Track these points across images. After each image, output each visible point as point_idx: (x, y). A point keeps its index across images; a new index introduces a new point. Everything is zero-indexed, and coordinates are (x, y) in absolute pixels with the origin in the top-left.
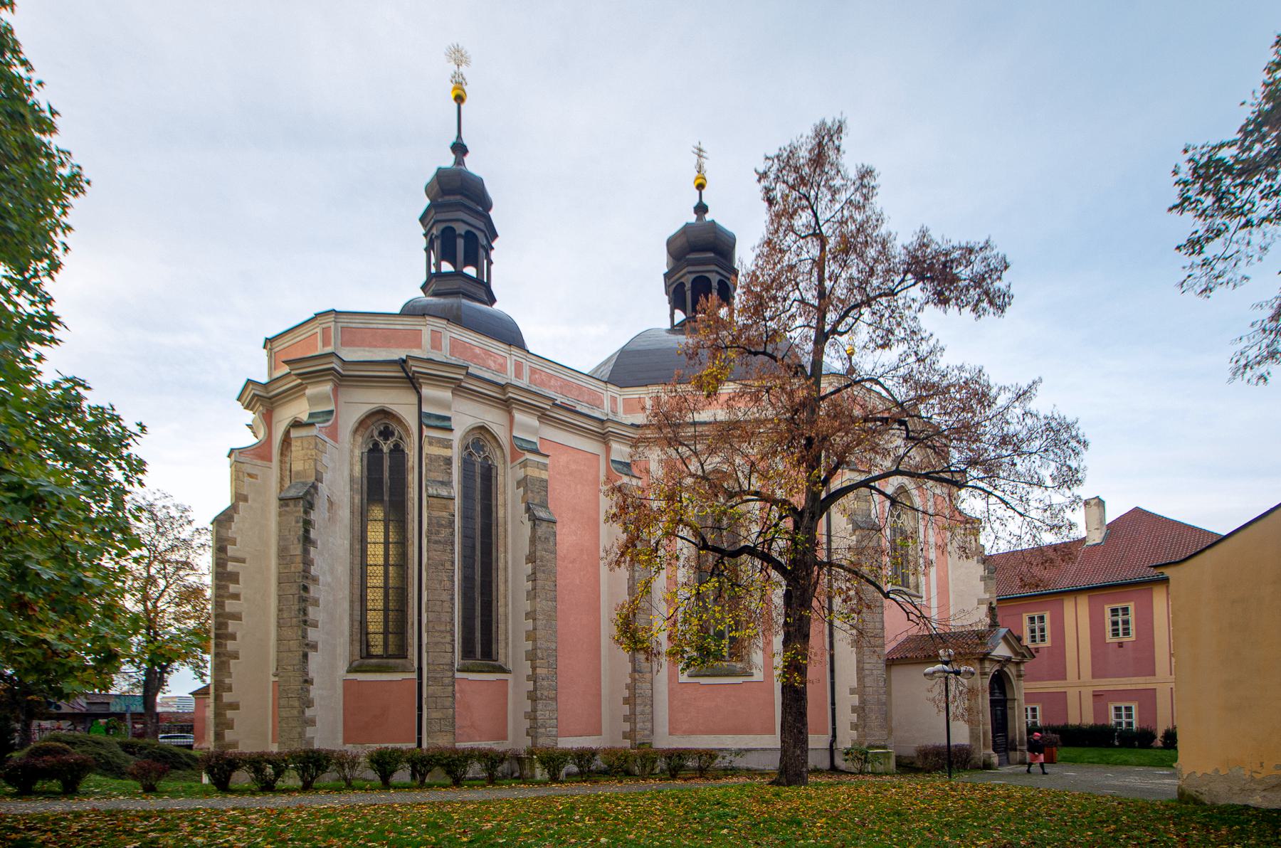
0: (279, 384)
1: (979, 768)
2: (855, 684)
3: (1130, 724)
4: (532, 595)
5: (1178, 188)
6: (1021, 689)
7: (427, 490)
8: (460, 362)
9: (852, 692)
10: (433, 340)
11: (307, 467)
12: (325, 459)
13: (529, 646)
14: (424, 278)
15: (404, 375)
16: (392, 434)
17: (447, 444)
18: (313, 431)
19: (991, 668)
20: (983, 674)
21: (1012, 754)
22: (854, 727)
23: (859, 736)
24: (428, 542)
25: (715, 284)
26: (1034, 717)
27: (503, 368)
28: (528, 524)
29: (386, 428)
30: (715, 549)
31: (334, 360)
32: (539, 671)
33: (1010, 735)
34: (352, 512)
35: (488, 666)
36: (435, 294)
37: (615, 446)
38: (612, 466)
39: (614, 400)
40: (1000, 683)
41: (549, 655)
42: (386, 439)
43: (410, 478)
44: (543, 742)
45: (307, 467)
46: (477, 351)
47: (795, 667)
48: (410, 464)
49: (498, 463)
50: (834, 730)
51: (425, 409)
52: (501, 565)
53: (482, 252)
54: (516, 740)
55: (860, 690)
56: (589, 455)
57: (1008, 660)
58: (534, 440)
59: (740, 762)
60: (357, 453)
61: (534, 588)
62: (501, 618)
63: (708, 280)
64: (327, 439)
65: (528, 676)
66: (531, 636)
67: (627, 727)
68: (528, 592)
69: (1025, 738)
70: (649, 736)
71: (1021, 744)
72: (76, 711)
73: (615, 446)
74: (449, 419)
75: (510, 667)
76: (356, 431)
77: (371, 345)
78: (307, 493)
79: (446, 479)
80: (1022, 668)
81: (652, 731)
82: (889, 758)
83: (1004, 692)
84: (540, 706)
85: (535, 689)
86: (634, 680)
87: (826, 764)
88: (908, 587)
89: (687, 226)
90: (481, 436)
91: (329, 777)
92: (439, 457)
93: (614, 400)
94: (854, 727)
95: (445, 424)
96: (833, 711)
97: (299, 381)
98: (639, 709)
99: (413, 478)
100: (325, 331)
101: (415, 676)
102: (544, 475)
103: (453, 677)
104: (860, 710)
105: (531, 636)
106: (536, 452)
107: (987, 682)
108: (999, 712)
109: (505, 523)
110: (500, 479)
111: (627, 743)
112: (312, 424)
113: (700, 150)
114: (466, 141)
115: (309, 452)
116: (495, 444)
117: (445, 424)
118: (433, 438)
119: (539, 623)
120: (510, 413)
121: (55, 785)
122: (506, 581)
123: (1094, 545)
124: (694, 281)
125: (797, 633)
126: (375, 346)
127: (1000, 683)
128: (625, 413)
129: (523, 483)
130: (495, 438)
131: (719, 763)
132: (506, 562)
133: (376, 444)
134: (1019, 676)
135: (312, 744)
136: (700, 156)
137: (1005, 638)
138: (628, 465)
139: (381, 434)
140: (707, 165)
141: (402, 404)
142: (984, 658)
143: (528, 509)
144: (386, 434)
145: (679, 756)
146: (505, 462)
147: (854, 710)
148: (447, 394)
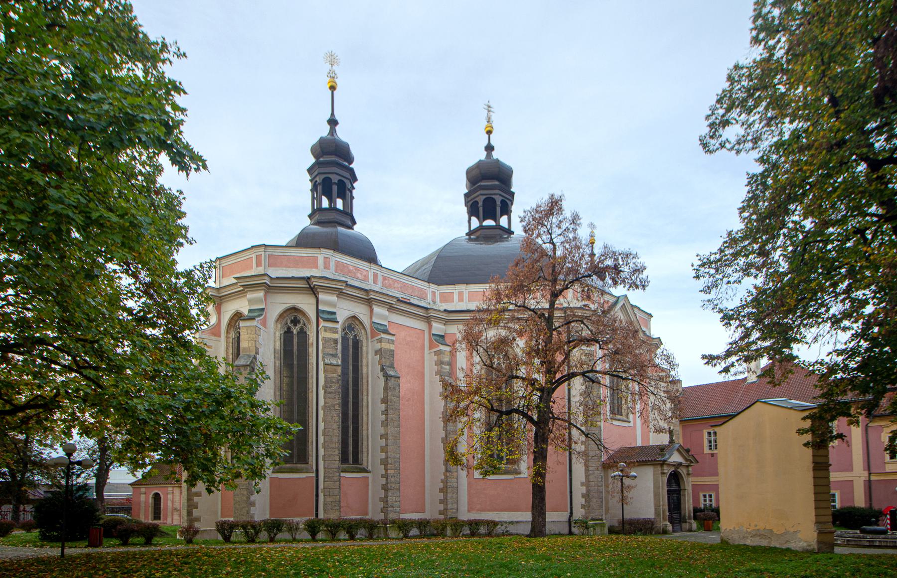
0: (224, 290)
1: (659, 533)
2: (584, 480)
3: (711, 505)
4: (385, 424)
5: (695, 272)
6: (689, 483)
7: (323, 360)
8: (344, 279)
9: (582, 484)
10: (325, 263)
11: (250, 345)
12: (260, 340)
13: (383, 455)
14: (310, 212)
15: (308, 286)
16: (299, 322)
17: (335, 331)
18: (254, 323)
19: (668, 470)
20: (663, 473)
21: (684, 525)
22: (583, 507)
23: (586, 513)
24: (325, 392)
25: (498, 203)
26: (711, 501)
27: (366, 279)
28: (383, 379)
29: (295, 318)
30: (497, 411)
31: (266, 278)
32: (389, 472)
33: (683, 513)
34: (275, 372)
35: (357, 468)
36: (318, 223)
37: (435, 325)
38: (433, 338)
39: (434, 293)
40: (675, 479)
41: (395, 462)
42: (295, 325)
43: (310, 350)
44: (391, 516)
45: (250, 345)
46: (351, 268)
47: (539, 475)
48: (311, 341)
49: (363, 338)
50: (571, 509)
51: (320, 308)
52: (364, 404)
53: (348, 192)
54: (374, 514)
55: (587, 484)
56: (418, 331)
57: (680, 464)
58: (385, 323)
59: (512, 529)
60: (278, 334)
61: (386, 420)
62: (365, 438)
63: (494, 201)
64: (261, 327)
65: (382, 475)
66: (384, 449)
67: (442, 507)
68: (382, 422)
69: (692, 515)
70: (455, 513)
71: (690, 518)
72: (37, 498)
73: (435, 325)
74: (334, 313)
75: (370, 468)
76: (277, 321)
77: (286, 266)
78: (252, 362)
79: (334, 352)
80: (690, 469)
81: (457, 510)
82: (604, 527)
83: (678, 484)
84: (390, 494)
85: (387, 483)
86: (446, 477)
87: (566, 531)
88: (622, 415)
89: (480, 162)
90: (353, 322)
91: (283, 535)
92: (330, 339)
93: (434, 293)
94: (583, 507)
95: (333, 316)
96: (571, 496)
97: (241, 288)
98: (449, 495)
99: (312, 350)
100: (258, 257)
101: (314, 475)
102: (392, 347)
103: (339, 476)
104: (586, 496)
105: (384, 449)
106: (386, 332)
107: (665, 479)
108: (675, 498)
109: (367, 377)
110: (364, 348)
111: (442, 517)
112: (253, 319)
113: (489, 107)
114: (337, 117)
115: (252, 336)
116: (361, 327)
117: (333, 316)
118: (327, 327)
119: (389, 441)
120: (371, 307)
121: (141, 540)
122: (368, 414)
123: (752, 383)
124: (485, 201)
125: (540, 456)
126: (289, 267)
127: (675, 479)
128: (441, 302)
129: (379, 352)
130: (361, 323)
131: (499, 529)
132: (368, 402)
133: (289, 328)
134: (688, 474)
135: (253, 518)
136: (489, 111)
137: (678, 450)
138: (442, 337)
139: (292, 322)
140: (494, 117)
141: (306, 304)
142: (663, 463)
143: (383, 369)
144: (295, 322)
145: (476, 524)
146: (367, 338)
147: (583, 496)
148: (333, 298)
